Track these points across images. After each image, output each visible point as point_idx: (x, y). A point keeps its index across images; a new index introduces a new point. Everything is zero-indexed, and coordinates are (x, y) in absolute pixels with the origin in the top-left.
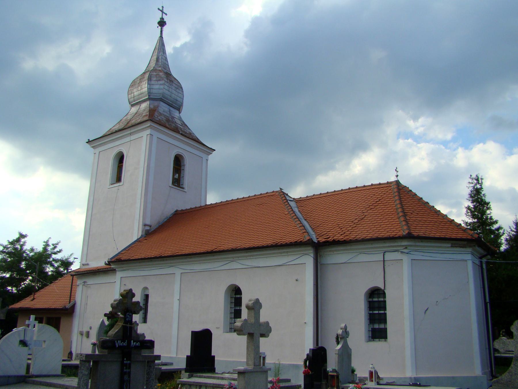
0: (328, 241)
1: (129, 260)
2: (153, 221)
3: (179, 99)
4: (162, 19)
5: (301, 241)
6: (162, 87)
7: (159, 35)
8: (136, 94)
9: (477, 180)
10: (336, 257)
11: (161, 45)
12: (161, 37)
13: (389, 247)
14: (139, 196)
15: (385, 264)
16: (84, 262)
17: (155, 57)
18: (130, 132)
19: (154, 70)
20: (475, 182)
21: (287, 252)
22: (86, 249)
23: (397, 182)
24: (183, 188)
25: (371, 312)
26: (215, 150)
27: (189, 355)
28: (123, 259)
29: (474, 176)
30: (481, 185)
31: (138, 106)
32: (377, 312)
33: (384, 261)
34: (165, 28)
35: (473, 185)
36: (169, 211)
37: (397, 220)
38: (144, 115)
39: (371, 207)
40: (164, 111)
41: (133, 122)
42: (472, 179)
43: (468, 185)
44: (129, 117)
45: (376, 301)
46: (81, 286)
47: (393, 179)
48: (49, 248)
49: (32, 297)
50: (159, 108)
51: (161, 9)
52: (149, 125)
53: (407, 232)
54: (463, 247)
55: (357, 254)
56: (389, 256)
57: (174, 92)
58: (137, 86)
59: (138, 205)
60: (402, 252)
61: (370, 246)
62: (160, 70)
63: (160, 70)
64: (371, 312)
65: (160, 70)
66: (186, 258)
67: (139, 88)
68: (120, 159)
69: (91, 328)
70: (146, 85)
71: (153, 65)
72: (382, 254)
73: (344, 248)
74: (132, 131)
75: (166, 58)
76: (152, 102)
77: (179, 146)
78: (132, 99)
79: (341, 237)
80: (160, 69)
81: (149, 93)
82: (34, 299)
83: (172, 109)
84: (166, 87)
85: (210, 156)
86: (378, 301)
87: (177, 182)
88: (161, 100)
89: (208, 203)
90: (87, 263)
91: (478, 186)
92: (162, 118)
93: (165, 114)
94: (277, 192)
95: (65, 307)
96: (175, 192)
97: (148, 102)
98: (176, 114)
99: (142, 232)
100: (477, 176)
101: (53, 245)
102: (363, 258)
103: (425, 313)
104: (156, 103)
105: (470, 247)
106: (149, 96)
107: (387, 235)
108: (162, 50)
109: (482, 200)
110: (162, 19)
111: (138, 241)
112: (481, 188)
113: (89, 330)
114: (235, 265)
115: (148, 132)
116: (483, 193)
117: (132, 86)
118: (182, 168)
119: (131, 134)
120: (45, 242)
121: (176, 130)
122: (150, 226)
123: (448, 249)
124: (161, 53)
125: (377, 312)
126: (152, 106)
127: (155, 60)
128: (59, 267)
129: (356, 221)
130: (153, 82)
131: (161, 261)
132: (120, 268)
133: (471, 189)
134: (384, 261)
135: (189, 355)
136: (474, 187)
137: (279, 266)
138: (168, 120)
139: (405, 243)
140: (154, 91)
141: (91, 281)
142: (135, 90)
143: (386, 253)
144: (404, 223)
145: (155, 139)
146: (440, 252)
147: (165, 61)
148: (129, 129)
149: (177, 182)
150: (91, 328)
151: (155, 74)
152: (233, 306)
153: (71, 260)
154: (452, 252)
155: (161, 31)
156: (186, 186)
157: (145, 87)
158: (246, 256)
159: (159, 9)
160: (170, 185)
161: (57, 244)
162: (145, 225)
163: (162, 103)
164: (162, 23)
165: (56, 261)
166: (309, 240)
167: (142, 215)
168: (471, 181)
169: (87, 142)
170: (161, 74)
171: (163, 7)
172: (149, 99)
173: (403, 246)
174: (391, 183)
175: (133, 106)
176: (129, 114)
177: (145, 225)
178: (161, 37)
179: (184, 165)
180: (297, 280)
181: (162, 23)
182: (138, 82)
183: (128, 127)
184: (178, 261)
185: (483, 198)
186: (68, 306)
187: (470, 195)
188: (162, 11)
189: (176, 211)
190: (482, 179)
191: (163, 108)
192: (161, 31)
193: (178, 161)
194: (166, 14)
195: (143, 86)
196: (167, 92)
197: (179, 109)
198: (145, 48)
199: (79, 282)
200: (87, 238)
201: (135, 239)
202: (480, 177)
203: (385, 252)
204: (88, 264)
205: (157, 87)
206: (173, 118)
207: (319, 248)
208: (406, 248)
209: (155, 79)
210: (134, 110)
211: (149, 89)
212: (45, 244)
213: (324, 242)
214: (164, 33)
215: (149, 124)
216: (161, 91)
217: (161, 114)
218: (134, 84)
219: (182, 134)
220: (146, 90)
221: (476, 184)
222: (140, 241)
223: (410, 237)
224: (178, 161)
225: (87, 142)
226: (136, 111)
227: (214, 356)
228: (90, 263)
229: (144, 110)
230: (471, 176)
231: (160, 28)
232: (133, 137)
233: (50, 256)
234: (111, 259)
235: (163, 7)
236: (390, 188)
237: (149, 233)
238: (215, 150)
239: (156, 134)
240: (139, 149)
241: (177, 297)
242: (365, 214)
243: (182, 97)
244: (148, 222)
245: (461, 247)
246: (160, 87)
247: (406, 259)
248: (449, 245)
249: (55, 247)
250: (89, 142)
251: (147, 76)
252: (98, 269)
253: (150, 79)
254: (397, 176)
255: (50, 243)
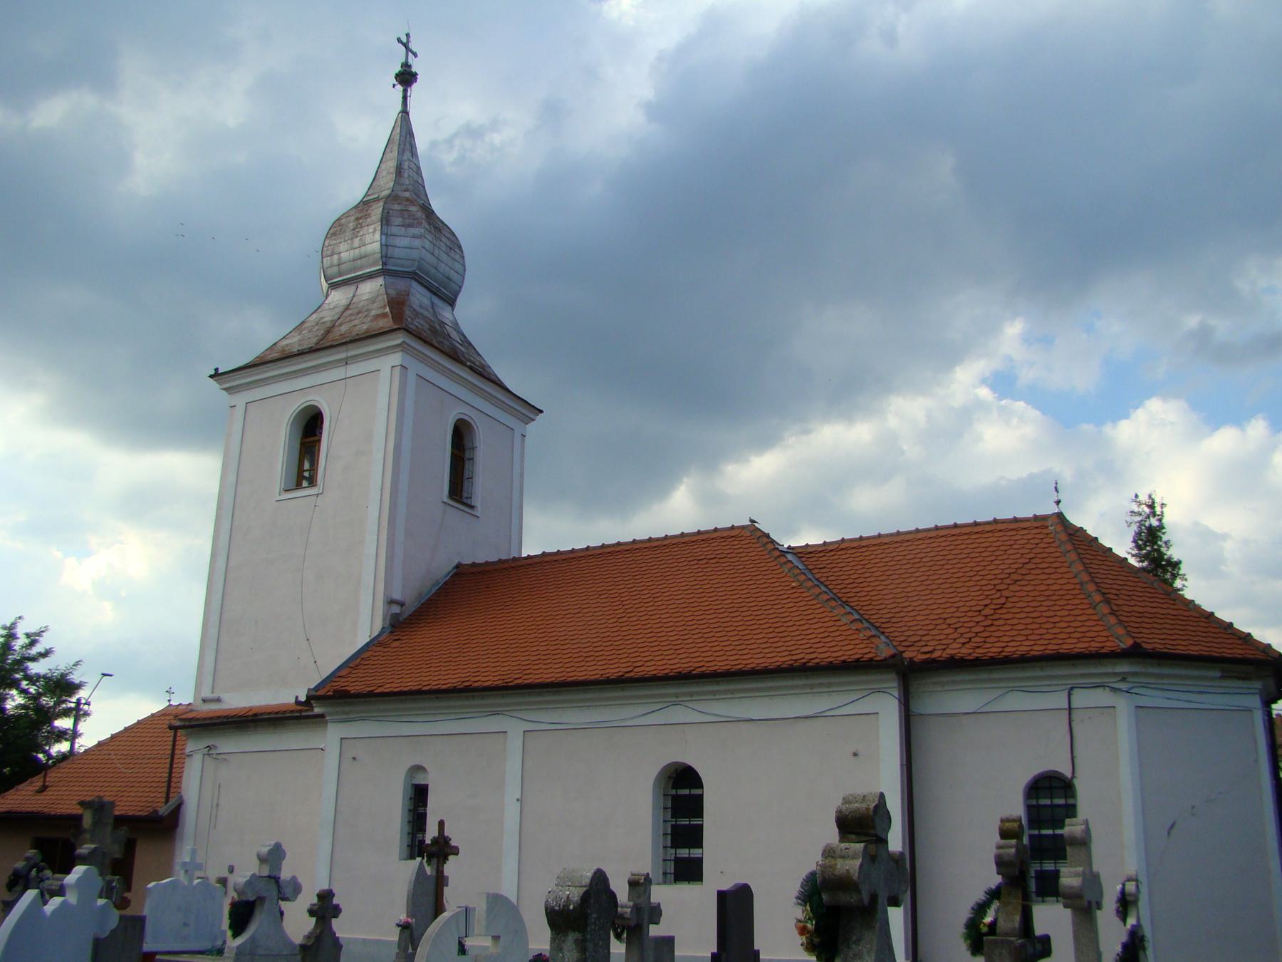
0: (934, 661)
1: (371, 695)
2: (409, 591)
3: (454, 275)
4: (406, 65)
5: (871, 659)
6: (417, 243)
7: (399, 108)
8: (345, 256)
9: (1152, 506)
10: (952, 700)
11: (404, 135)
12: (405, 112)
13: (1083, 675)
14: (371, 525)
15: (1073, 717)
16: (206, 693)
17: (391, 164)
18: (343, 355)
19: (393, 197)
20: (1147, 510)
21: (829, 685)
22: (210, 659)
23: (1060, 516)
24: (472, 507)
25: (1036, 832)
26: (541, 411)
27: (715, 950)
28: (353, 689)
29: (1143, 498)
30: (1160, 520)
31: (353, 288)
32: (1050, 832)
33: (1070, 709)
34: (415, 89)
35: (1139, 519)
36: (442, 566)
37: (1090, 611)
38: (373, 313)
39: (1014, 577)
40: (421, 306)
41: (344, 329)
42: (1140, 504)
43: (1129, 519)
44: (328, 316)
45: (1045, 806)
46: (198, 758)
47: (1053, 509)
48: (18, 644)
49: (37, 782)
50: (412, 298)
51: (404, 40)
52: (399, 341)
53: (1130, 642)
54: (1243, 679)
55: (1000, 692)
56: (1082, 698)
57: (444, 257)
58: (348, 234)
59: (370, 548)
60: (1114, 690)
61: (1039, 673)
62: (402, 195)
63: (407, 200)
64: (1036, 832)
65: (402, 195)
66: (540, 694)
67: (357, 242)
68: (310, 427)
69: (231, 870)
70: (377, 236)
71: (387, 183)
72: (1066, 693)
73: (973, 677)
74: (350, 354)
75: (419, 168)
76: (391, 280)
77: (465, 400)
78: (335, 270)
79: (964, 651)
80: (407, 194)
81: (385, 258)
82: (44, 788)
83: (436, 300)
84: (427, 244)
85: (531, 427)
86: (1052, 806)
87: (459, 488)
88: (414, 276)
89: (531, 548)
90: (215, 696)
91: (1154, 522)
92: (417, 323)
93: (426, 313)
94: (743, 527)
95: (156, 812)
96: (455, 516)
97: (380, 281)
98: (446, 314)
99: (384, 619)
100: (1150, 496)
101: (28, 635)
102: (1017, 701)
103: (1169, 833)
104: (402, 284)
105: (1259, 678)
106: (384, 264)
107: (1080, 647)
108: (408, 146)
109: (1161, 554)
110: (406, 65)
111: (374, 644)
112: (1161, 527)
113: (225, 874)
114: (679, 714)
115: (396, 358)
116: (1164, 538)
117: (334, 234)
118: (467, 455)
119: (346, 362)
120: (5, 628)
121: (454, 356)
122: (402, 604)
123: (1216, 684)
124: (407, 155)
125: (1050, 832)
126: (393, 292)
127: (393, 170)
128: (40, 695)
129: (987, 611)
130: (394, 230)
131: (467, 698)
132: (337, 713)
133: (1135, 528)
134: (1070, 709)
135: (715, 950)
136: (1141, 523)
137: (806, 717)
138: (433, 331)
139: (1123, 667)
140: (396, 253)
141: (229, 744)
142: (343, 247)
143: (1076, 692)
144: (1112, 620)
145: (412, 378)
146: (1196, 689)
147: (415, 176)
148: (344, 348)
149: (459, 488)
150: (231, 870)
151: (397, 207)
152: (669, 817)
153: (75, 678)
154: (1196, 689)
155: (405, 98)
156: (477, 501)
157: (372, 240)
158: (714, 693)
159: (399, 40)
160: (446, 500)
161: (39, 634)
162: (391, 602)
163: (414, 284)
164: (406, 78)
165: (33, 680)
166: (893, 656)
167: (382, 575)
168: (1136, 510)
169: (211, 376)
170: (413, 209)
171: (408, 35)
172: (384, 272)
173: (1115, 674)
174: (1045, 518)
175: (333, 286)
176: (326, 306)
177: (391, 602)
178: (405, 112)
179: (473, 448)
180: (855, 755)
181: (406, 78)
182: (351, 225)
183: (328, 344)
184: (515, 700)
185: (1163, 550)
186: (163, 810)
187: (1135, 541)
188: (406, 45)
189: (458, 566)
190: (1163, 505)
191: (419, 297)
192: (405, 98)
193: (461, 436)
194: (415, 55)
195: (368, 239)
196: (429, 257)
197: (452, 303)
198: (361, 139)
199: (193, 746)
200: (213, 631)
201: (363, 639)
202: (1157, 500)
203: (1072, 689)
204: (218, 700)
205: (404, 242)
206: (442, 324)
207: (911, 673)
208: (1124, 680)
209: (398, 221)
210: (339, 297)
211: (385, 246)
212: (5, 632)
213: (925, 662)
214: (412, 102)
215: (399, 339)
216: (415, 254)
217: (417, 314)
218: (337, 229)
219: (471, 368)
220: (376, 247)
221: (1148, 517)
222: (380, 644)
223: (1135, 653)
224: (461, 436)
225: (211, 376)
226: (344, 302)
227: (758, 952)
228: (222, 696)
229: (373, 301)
230: (1137, 496)
231: (400, 88)
232: (354, 369)
233: (20, 663)
234: (317, 688)
235: (408, 35)
236: (1045, 531)
237: (405, 622)
238: (541, 411)
239: (416, 367)
240: (371, 405)
241: (513, 791)
242: (1006, 593)
243: (461, 271)
244: (397, 596)
245: (1239, 678)
246: (412, 245)
247: (1123, 705)
248: (1218, 674)
249: (33, 643)
250: (216, 375)
251: (377, 211)
252: (255, 715)
253: (386, 220)
254: (1058, 502)
255: (21, 631)
